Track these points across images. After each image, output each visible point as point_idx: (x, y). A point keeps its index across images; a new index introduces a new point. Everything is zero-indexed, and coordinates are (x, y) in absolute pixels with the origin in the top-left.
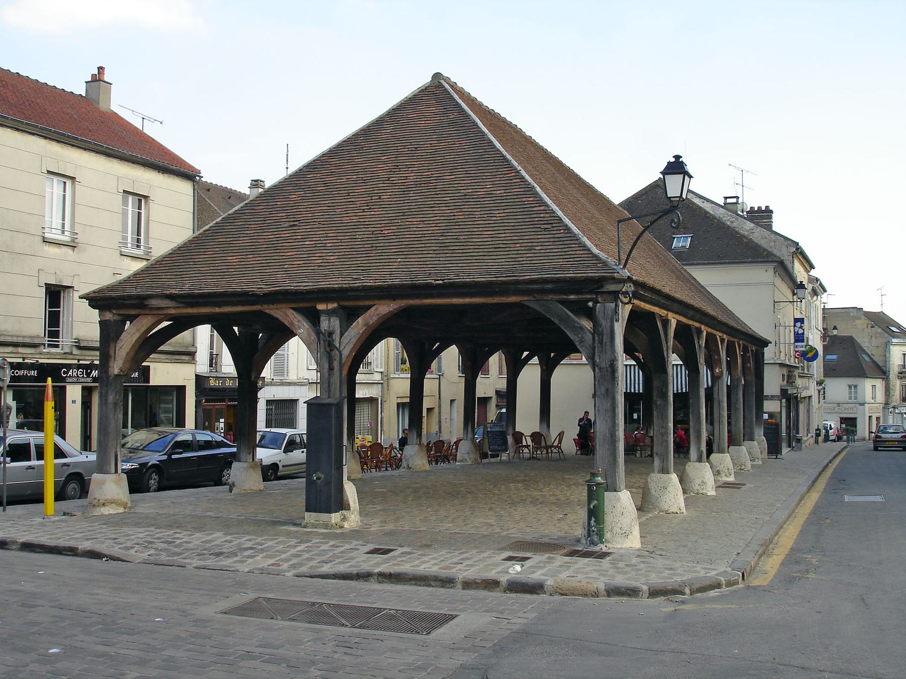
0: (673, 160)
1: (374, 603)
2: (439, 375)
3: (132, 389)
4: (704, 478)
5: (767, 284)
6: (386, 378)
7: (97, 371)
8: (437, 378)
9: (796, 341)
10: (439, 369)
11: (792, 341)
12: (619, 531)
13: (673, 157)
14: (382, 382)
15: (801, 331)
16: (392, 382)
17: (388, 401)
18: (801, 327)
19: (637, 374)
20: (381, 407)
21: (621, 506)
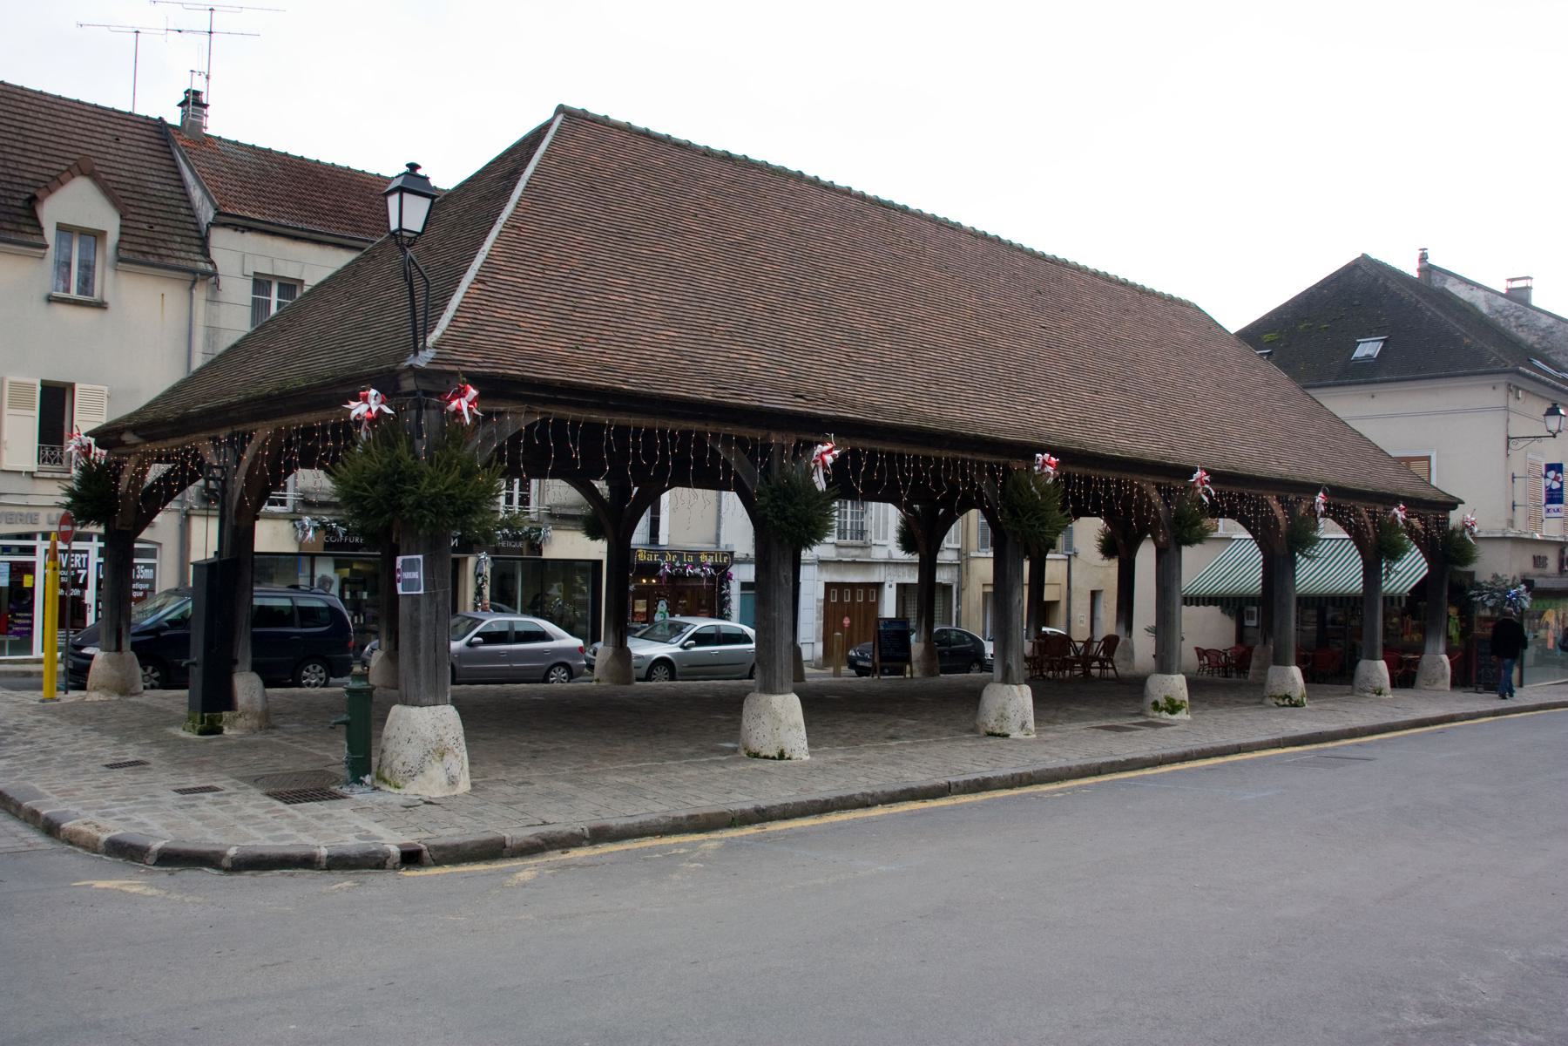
0: (406, 169)
1: (244, 841)
2: (1069, 556)
3: (522, 564)
4: (1005, 709)
5: (1496, 409)
6: (964, 558)
7: (452, 544)
8: (1065, 560)
9: (1550, 500)
10: (1069, 546)
11: (1544, 501)
12: (400, 767)
13: (407, 165)
14: (959, 562)
15: (1556, 485)
16: (973, 563)
17: (967, 589)
18: (1556, 479)
19: (1256, 557)
20: (957, 597)
21: (408, 729)
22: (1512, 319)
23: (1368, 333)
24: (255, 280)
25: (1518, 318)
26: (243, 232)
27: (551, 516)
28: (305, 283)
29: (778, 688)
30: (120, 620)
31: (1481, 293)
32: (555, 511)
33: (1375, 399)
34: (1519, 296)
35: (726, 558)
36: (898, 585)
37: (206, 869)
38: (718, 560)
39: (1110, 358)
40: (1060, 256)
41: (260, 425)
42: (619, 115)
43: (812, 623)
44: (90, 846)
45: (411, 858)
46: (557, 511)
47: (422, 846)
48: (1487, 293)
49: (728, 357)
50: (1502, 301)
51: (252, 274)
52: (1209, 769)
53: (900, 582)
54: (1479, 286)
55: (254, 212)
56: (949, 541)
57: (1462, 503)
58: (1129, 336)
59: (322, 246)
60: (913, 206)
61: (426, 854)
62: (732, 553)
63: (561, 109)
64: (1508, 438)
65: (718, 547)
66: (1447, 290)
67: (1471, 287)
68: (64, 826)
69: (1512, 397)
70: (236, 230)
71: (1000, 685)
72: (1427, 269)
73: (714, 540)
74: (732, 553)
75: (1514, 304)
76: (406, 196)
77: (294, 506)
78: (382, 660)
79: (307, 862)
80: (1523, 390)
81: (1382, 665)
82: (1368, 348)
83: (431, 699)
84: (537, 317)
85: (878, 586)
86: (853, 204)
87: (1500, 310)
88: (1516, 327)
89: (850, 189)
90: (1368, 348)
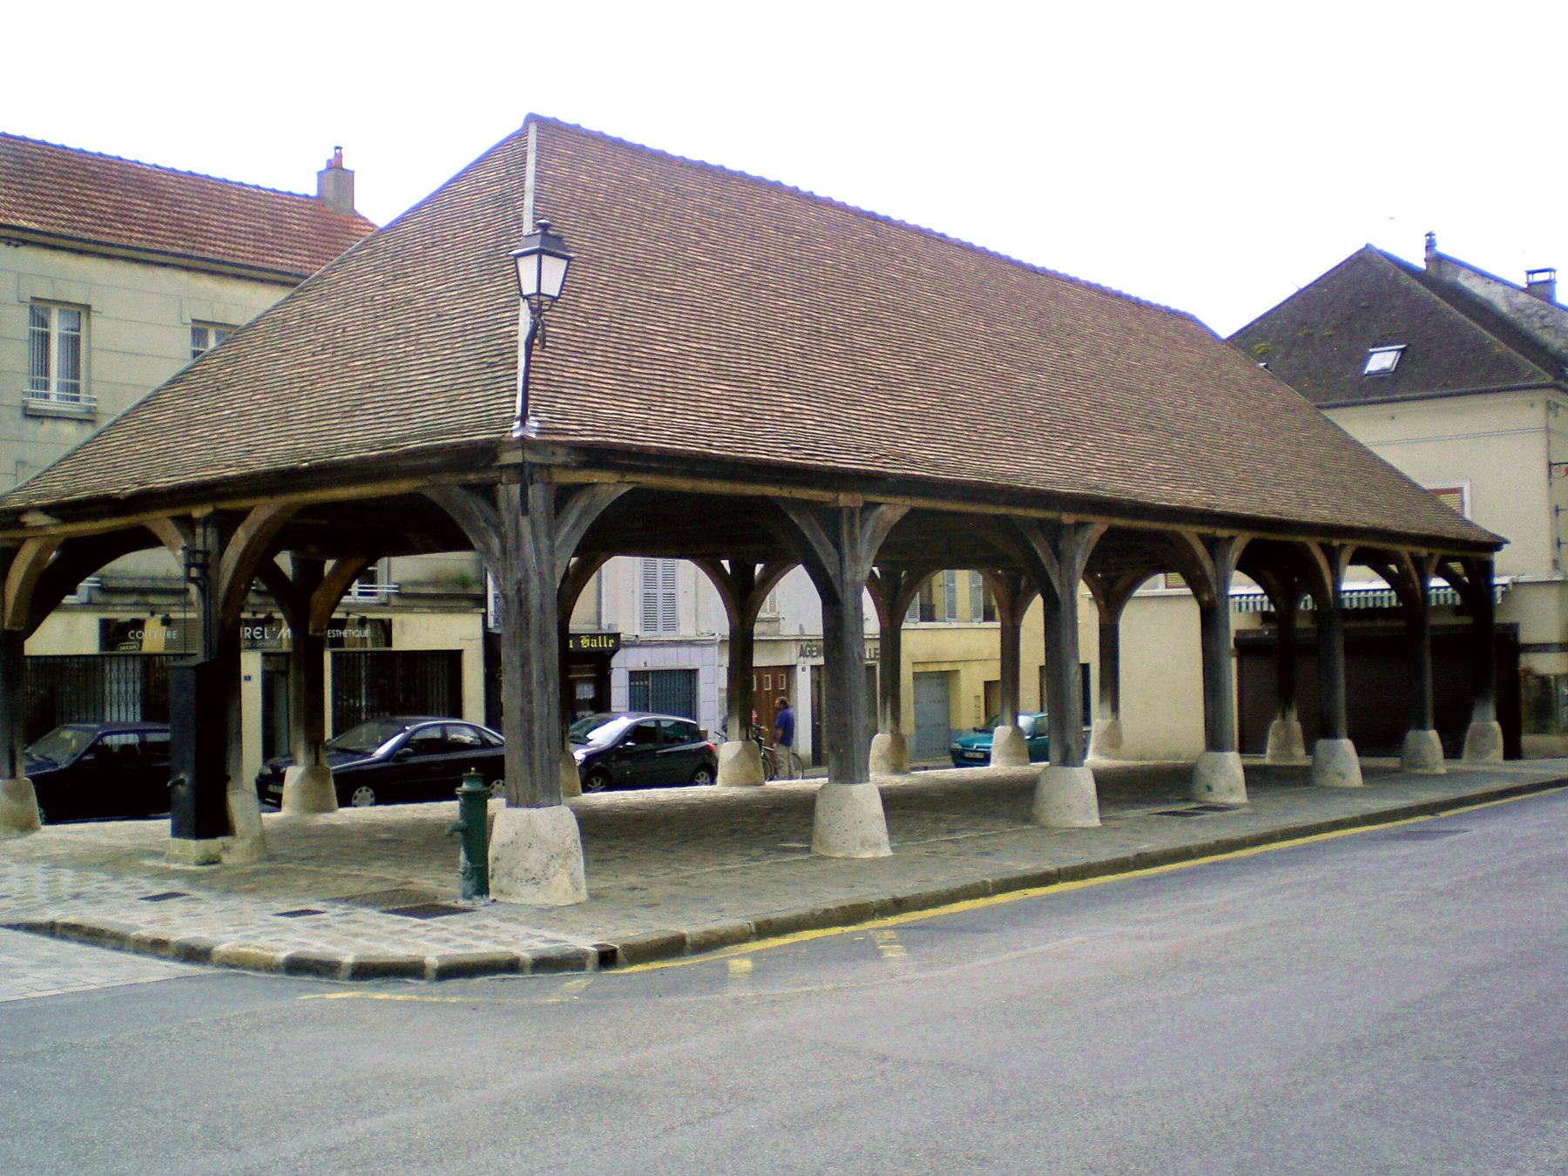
22: (1535, 319)
23: (1381, 342)
24: (194, 331)
25: (1543, 317)
26: (17, 246)
27: (400, 595)
28: (93, 308)
29: (857, 777)
30: (12, 738)
31: (1500, 288)
32: (404, 590)
33: (1394, 422)
34: (1541, 290)
35: (611, 641)
36: (812, 667)
37: (409, 980)
38: (603, 643)
39: (1128, 390)
40: (1050, 268)
41: (261, 501)
42: (591, 124)
43: (714, 720)
44: (270, 967)
45: (607, 958)
46: (409, 590)
47: (617, 946)
48: (1507, 288)
49: (783, 412)
50: (1523, 298)
51: (28, 299)
52: (1172, 875)
53: (813, 664)
54: (1497, 280)
55: (30, 221)
56: (765, 611)
57: (1507, 542)
58: (1139, 361)
59: (111, 261)
60: (896, 217)
61: (620, 953)
62: (618, 635)
63: (531, 118)
64: (1550, 465)
65: (600, 628)
66: (1460, 285)
67: (1488, 280)
68: (215, 949)
69: (1552, 416)
70: (9, 244)
71: (1059, 768)
72: (1437, 260)
73: (594, 619)
74: (618, 635)
75: (1537, 301)
76: (545, 258)
77: (89, 594)
78: (302, 778)
79: (512, 966)
80: (1563, 407)
81: (1433, 734)
82: (1382, 360)
83: (546, 800)
84: (601, 375)
85: (789, 669)
86: (838, 217)
87: (1523, 307)
88: (1540, 328)
89: (797, 188)
90: (1382, 360)
